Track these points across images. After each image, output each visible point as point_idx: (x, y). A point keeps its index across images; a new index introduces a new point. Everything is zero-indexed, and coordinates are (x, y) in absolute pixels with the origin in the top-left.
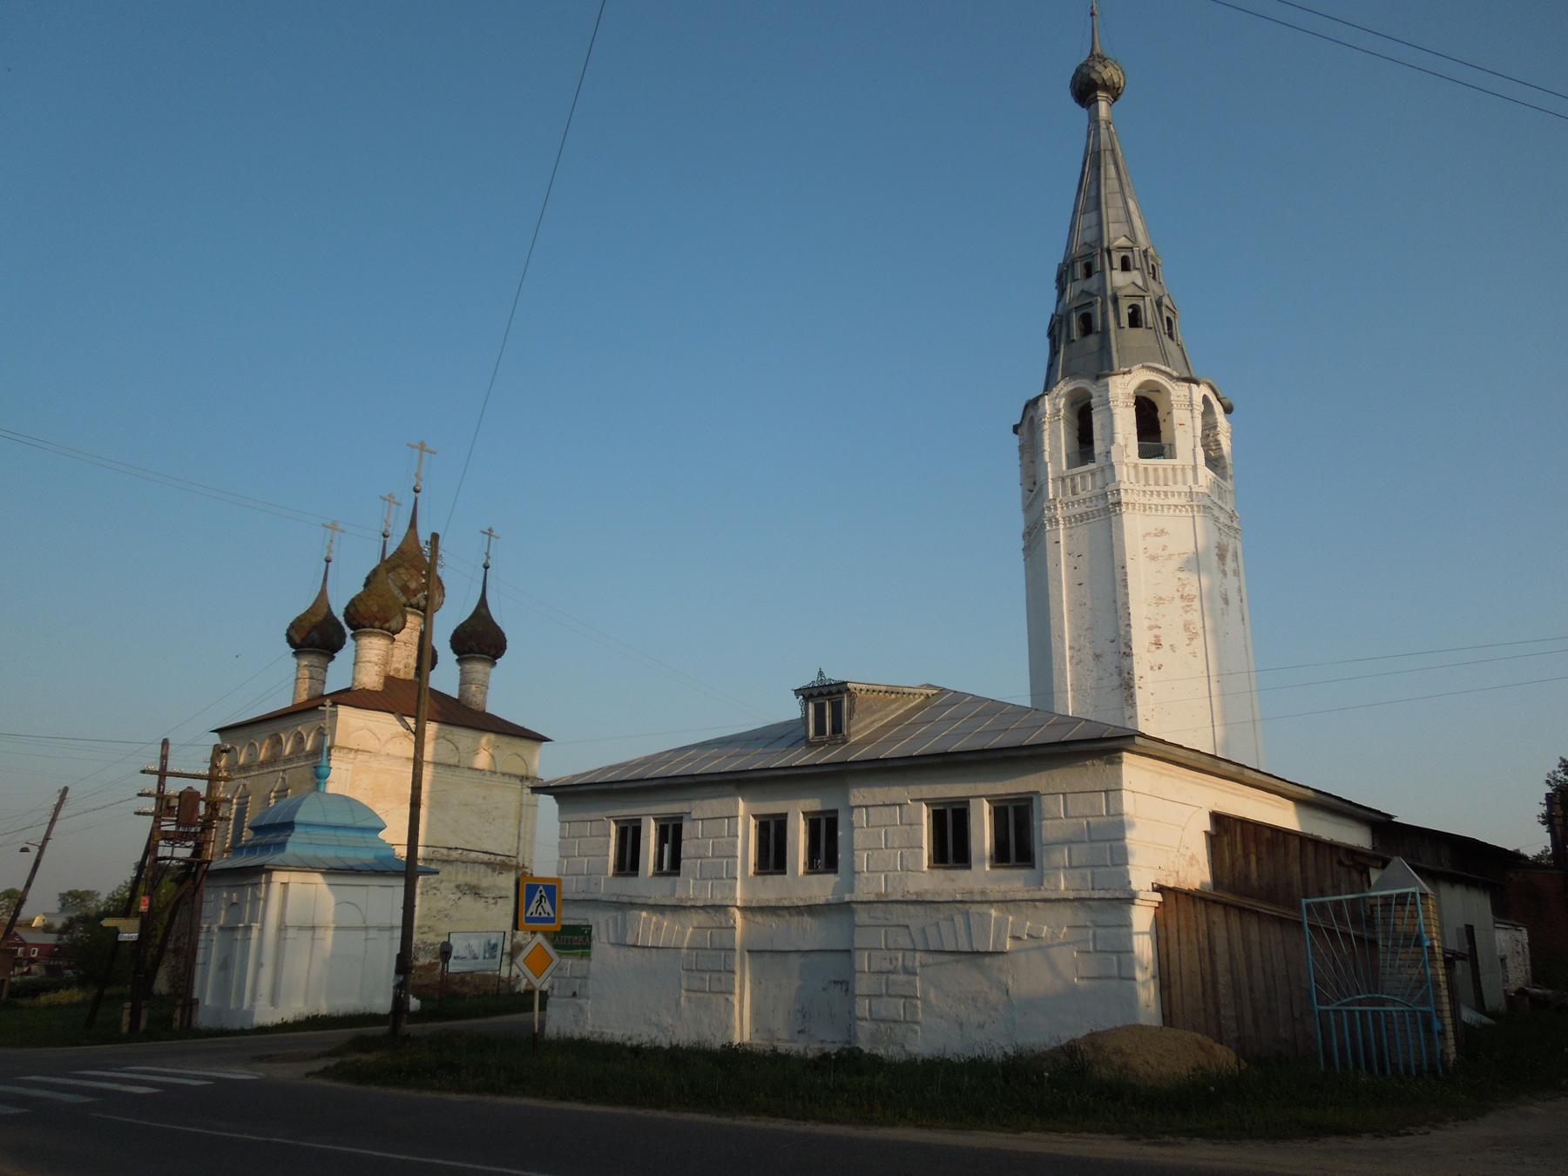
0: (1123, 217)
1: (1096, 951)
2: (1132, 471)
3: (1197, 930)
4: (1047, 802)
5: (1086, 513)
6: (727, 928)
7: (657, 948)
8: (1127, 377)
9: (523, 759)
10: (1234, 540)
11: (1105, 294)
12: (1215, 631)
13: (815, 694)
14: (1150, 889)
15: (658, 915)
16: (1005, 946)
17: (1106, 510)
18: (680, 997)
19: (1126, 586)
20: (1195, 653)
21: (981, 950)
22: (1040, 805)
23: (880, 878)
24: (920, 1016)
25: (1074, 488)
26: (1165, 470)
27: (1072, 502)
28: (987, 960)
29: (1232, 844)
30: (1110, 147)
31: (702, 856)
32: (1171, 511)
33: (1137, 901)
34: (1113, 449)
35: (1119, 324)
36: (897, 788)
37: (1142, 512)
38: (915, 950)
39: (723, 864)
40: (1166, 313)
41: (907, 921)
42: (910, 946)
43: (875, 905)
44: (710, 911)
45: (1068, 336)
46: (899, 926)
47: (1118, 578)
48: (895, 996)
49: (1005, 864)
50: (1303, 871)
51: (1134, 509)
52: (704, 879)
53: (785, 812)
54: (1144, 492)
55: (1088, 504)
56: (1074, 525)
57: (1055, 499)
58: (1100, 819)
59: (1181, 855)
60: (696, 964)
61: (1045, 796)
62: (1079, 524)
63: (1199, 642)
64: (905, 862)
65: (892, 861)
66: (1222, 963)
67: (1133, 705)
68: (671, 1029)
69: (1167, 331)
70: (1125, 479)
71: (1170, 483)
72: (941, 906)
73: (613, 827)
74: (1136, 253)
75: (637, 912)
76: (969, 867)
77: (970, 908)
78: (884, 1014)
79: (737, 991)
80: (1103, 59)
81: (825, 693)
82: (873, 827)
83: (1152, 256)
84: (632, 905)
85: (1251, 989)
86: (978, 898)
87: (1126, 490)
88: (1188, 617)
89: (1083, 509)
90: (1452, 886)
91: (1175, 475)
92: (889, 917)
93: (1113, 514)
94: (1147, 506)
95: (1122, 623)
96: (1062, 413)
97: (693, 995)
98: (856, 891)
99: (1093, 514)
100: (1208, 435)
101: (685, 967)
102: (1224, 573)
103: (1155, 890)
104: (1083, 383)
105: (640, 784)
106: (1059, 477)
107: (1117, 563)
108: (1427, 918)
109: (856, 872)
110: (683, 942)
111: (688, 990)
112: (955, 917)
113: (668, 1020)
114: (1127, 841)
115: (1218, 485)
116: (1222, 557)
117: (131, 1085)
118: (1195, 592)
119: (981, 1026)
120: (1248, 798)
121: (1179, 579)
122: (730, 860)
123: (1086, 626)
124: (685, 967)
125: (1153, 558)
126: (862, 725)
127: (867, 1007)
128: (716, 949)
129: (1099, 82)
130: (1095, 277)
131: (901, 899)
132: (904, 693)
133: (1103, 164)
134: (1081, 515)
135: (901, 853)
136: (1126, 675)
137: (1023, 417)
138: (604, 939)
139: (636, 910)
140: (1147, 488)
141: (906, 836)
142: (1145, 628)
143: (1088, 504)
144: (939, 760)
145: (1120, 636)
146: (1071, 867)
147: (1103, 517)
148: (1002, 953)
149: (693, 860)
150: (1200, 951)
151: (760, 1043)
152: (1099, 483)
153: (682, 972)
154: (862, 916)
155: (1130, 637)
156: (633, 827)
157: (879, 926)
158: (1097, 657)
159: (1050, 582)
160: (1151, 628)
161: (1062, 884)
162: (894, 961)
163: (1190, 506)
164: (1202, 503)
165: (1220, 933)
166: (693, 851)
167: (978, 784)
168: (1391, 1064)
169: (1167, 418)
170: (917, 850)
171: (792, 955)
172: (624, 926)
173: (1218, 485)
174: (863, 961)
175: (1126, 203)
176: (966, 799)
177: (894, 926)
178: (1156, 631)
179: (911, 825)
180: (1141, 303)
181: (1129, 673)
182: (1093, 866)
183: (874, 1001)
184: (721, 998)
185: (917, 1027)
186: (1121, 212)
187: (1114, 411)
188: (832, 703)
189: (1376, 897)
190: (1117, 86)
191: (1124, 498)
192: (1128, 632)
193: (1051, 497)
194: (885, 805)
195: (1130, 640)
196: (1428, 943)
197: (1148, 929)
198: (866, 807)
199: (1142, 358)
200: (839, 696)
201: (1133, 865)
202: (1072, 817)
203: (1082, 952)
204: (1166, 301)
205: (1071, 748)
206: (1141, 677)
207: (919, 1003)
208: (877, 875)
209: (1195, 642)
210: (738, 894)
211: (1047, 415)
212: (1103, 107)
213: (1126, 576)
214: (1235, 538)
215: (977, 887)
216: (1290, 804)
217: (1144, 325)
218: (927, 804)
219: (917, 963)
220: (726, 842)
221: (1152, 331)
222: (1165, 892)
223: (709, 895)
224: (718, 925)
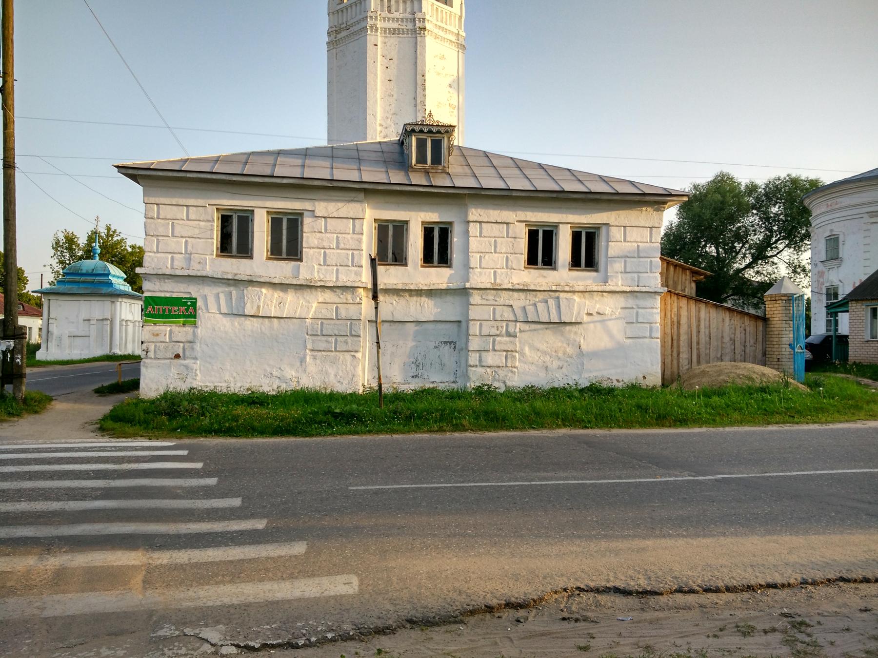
4: (614, 231)
5: (399, 29)
13: (426, 131)
15: (279, 292)
17: (414, 31)
19: (424, 90)
28: (568, 328)
38: (516, 321)
41: (511, 303)
42: (514, 319)
43: (489, 291)
44: (337, 290)
47: (419, 82)
49: (445, 265)
55: (400, 22)
58: (646, 244)
66: (684, 328)
72: (538, 293)
81: (434, 131)
85: (698, 343)
89: (395, 25)
92: (498, 299)
99: (403, 32)
101: (309, 333)
109: (470, 268)
110: (308, 312)
112: (549, 300)
117: (67, 463)
123: (392, 112)
124: (309, 333)
131: (511, 288)
138: (213, 308)
143: (400, 22)
146: (626, 272)
150: (672, 322)
154: (475, 298)
161: (618, 283)
165: (684, 313)
167: (568, 215)
174: (474, 328)
176: (556, 224)
184: (348, 356)
194: (497, 223)
198: (480, 222)
200: (439, 135)
202: (628, 242)
205: (647, 198)
219: (518, 330)
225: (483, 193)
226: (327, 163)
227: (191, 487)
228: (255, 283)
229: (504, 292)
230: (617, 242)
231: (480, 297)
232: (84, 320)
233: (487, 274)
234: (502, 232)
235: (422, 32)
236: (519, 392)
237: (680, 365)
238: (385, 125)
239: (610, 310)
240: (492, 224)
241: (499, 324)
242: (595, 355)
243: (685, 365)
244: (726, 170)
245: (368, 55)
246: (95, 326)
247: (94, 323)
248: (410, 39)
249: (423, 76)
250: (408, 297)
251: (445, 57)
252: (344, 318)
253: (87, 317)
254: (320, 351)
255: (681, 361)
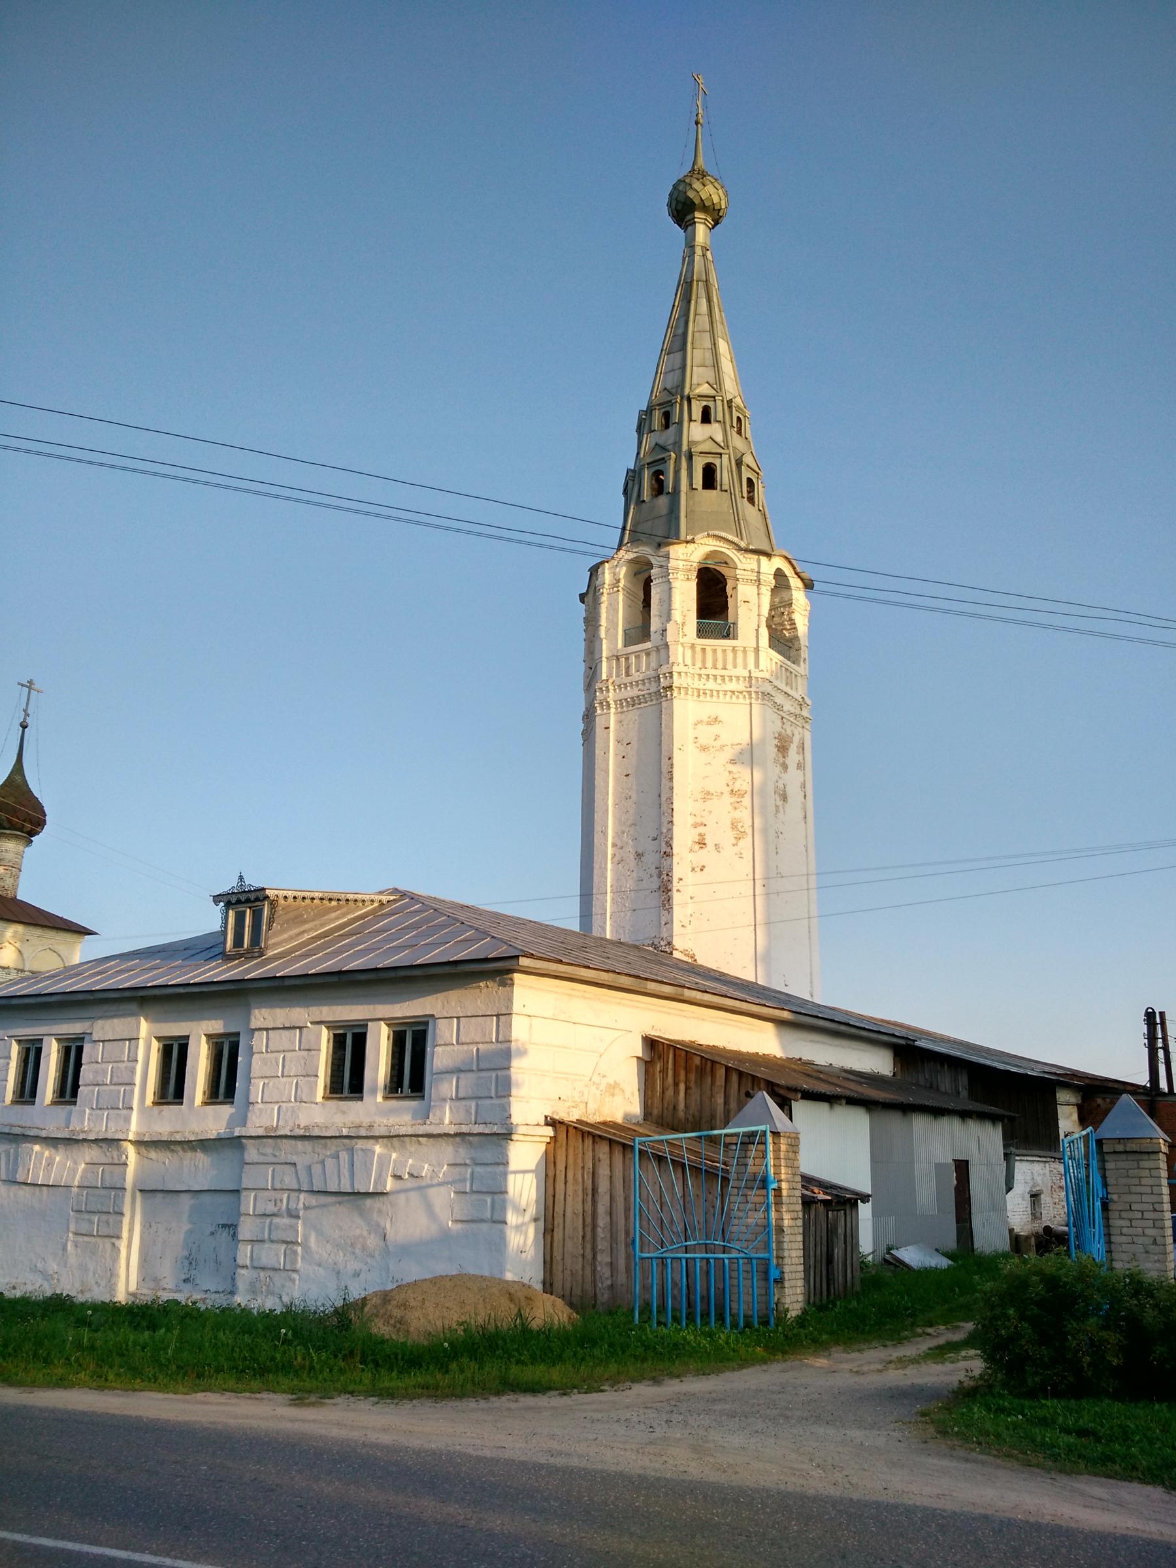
0: (709, 362)
1: (473, 1192)
2: (689, 653)
3: (583, 1168)
5: (638, 697)
6: (119, 1164)
7: (48, 1186)
8: (691, 547)
9: (59, 955)
10: (800, 729)
11: (680, 450)
12: (765, 831)
14: (542, 1122)
15: (52, 1149)
16: (385, 1186)
17: (658, 693)
18: (67, 1241)
19: (671, 779)
20: (741, 854)
21: (361, 1191)
22: (434, 1029)
23: (273, 1109)
24: (299, 1264)
25: (628, 668)
26: (724, 651)
27: (625, 684)
28: (369, 1202)
29: (664, 1071)
30: (704, 278)
31: (100, 1083)
32: (728, 697)
33: (514, 1137)
34: (669, 626)
35: (691, 484)
36: (298, 1010)
37: (695, 697)
38: (300, 1191)
39: (119, 1092)
40: (746, 474)
41: (294, 1159)
42: (296, 1187)
43: (265, 1140)
44: (104, 1145)
45: (639, 495)
46: (286, 1163)
47: (664, 769)
48: (277, 1242)
50: (726, 1103)
51: (687, 694)
52: (100, 1109)
53: (188, 1034)
54: (700, 675)
55: (640, 687)
56: (625, 709)
57: (607, 680)
59: (594, 1083)
60: (86, 1205)
61: (440, 1020)
62: (631, 708)
63: (746, 843)
64: (299, 1092)
65: (286, 1092)
67: (670, 910)
68: (56, 1276)
69: (745, 494)
70: (680, 660)
71: (729, 666)
72: (328, 1141)
73: (15, 1049)
74: (719, 403)
75: (29, 1145)
76: (361, 1099)
77: (356, 1144)
78: (264, 1261)
79: (125, 1234)
80: (703, 174)
82: (272, 1052)
83: (738, 407)
84: (25, 1138)
86: (363, 1133)
87: (679, 673)
88: (737, 814)
90: (935, 1118)
91: (735, 658)
92: (277, 1154)
93: (664, 699)
94: (701, 692)
95: (665, 820)
96: (621, 584)
97: (80, 1239)
98: (249, 1124)
100: (783, 613)
102: (785, 767)
103: (547, 1124)
104: (646, 551)
105: (39, 1000)
106: (613, 656)
107: (665, 753)
108: (777, 1158)
110: (74, 1179)
111: (76, 1234)
113: (53, 1266)
114: (512, 1070)
115: (786, 669)
116: (783, 749)
118: (746, 787)
119: (357, 1274)
120: (703, 1020)
121: (730, 772)
122: (128, 1088)
123: (629, 823)
124: (74, 1209)
125: (704, 749)
126: (285, 936)
127: (249, 1255)
128: (106, 1188)
129: (697, 201)
130: (672, 428)
132: (347, 900)
133: (694, 298)
134: (632, 698)
135: (297, 1082)
136: (664, 876)
137: (589, 587)
139: (30, 1143)
140: (703, 671)
141: (302, 1062)
142: (689, 825)
143: (640, 687)
144: (335, 979)
145: (662, 833)
146: (458, 1099)
147: (654, 702)
148: (382, 1194)
149: (90, 1088)
151: (146, 1296)
152: (654, 665)
153: (72, 1213)
154: (252, 1153)
155: (672, 835)
157: (268, 1163)
158: (639, 855)
159: (597, 772)
160: (695, 826)
162: (278, 1203)
163: (748, 692)
164: (760, 690)
166: (91, 1077)
167: (377, 1006)
168: (730, 1314)
169: (733, 593)
170: (312, 1079)
171: (183, 1195)
172: (16, 1158)
173: (786, 669)
174: (249, 1203)
175: (714, 344)
176: (365, 1023)
177: (282, 1164)
178: (701, 829)
179: (309, 1050)
180: (717, 462)
182: (480, 1098)
183: (257, 1246)
185: (295, 1276)
186: (708, 355)
187: (673, 585)
188: (254, 911)
189: (737, 1135)
190: (717, 207)
191: (677, 681)
192: (670, 830)
193: (604, 677)
194: (284, 1028)
195: (671, 838)
196: (775, 1186)
197: (532, 1166)
198: (267, 1029)
199: (707, 525)
201: (515, 1097)
202: (463, 1044)
203: (460, 1192)
204: (748, 459)
205: (383, 975)
206: (681, 879)
207: (299, 1249)
208: (271, 1105)
209: (741, 843)
210: (134, 1126)
211: (606, 586)
212: (701, 232)
213: (672, 768)
214: (803, 727)
215: (366, 1121)
216: (769, 1026)
217: (719, 488)
218: (328, 1028)
219: (301, 1205)
220: (126, 1068)
221: (727, 495)
222: (558, 1125)
223: (103, 1127)
224: (110, 1161)
225: (250, 986)
227: (803, 1497)
228: (30, 1138)
229: (284, 1141)
230: (446, 1045)
231: (256, 1151)
233: (268, 1112)
234: (293, 1043)
235: (669, 693)
236: (320, 1320)
237: (598, 1276)
238: (619, 845)
239: (431, 1169)
240: (281, 1031)
241: (277, 1195)
242: (406, 1250)
243: (607, 1279)
245: (596, 745)
248: (654, 707)
250: (181, 1153)
251: (719, 719)
252: (109, 1186)
254: (82, 1235)
255: (599, 1269)
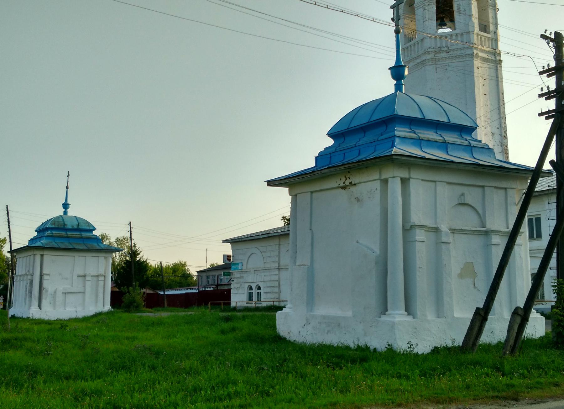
123: (487, 117)
156: (535, 218)
181: (506, 147)
192: (506, 126)
213: (504, 98)
226: (500, 150)
232: (79, 276)
244: (549, 161)
246: (90, 282)
247: (90, 279)
249: (503, 94)
253: (82, 273)
